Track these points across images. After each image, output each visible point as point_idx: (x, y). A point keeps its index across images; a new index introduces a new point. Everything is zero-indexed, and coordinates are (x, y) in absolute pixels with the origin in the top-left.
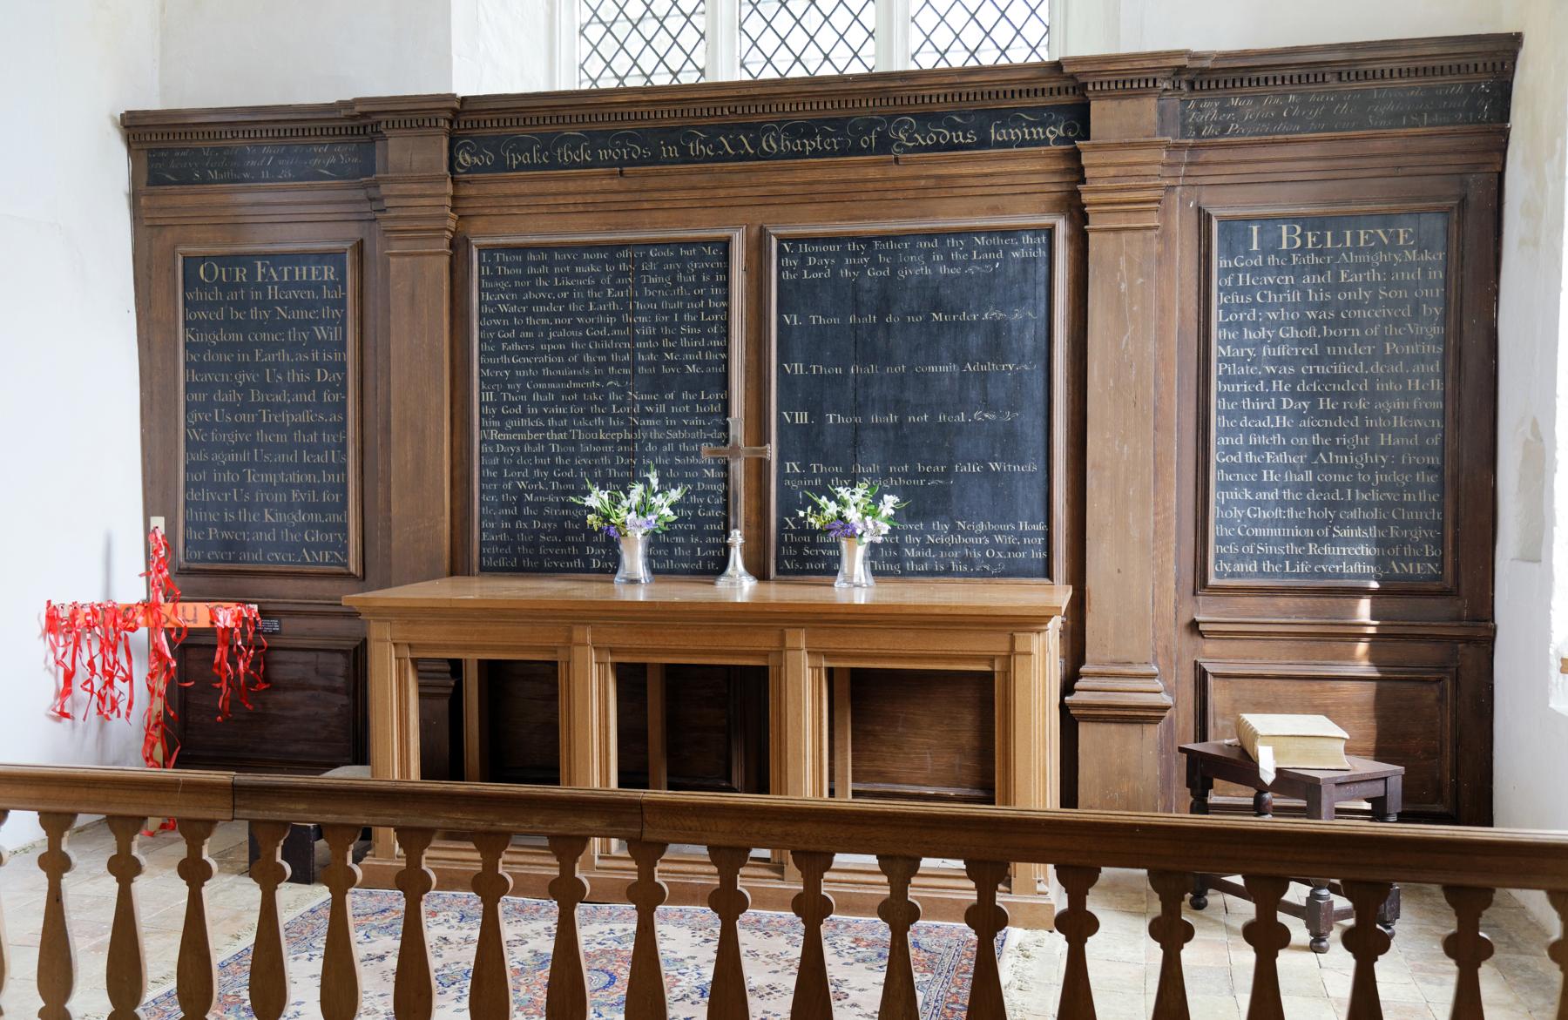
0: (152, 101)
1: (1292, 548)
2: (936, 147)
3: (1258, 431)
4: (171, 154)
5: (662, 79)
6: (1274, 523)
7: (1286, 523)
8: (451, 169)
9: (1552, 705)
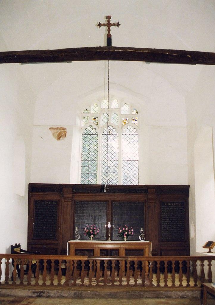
0: (190, 186)
1: (170, 237)
2: (131, 193)
3: (166, 224)
4: (33, 188)
5: (114, 184)
6: (168, 234)
7: (169, 234)
8: (72, 192)
9: (197, 251)
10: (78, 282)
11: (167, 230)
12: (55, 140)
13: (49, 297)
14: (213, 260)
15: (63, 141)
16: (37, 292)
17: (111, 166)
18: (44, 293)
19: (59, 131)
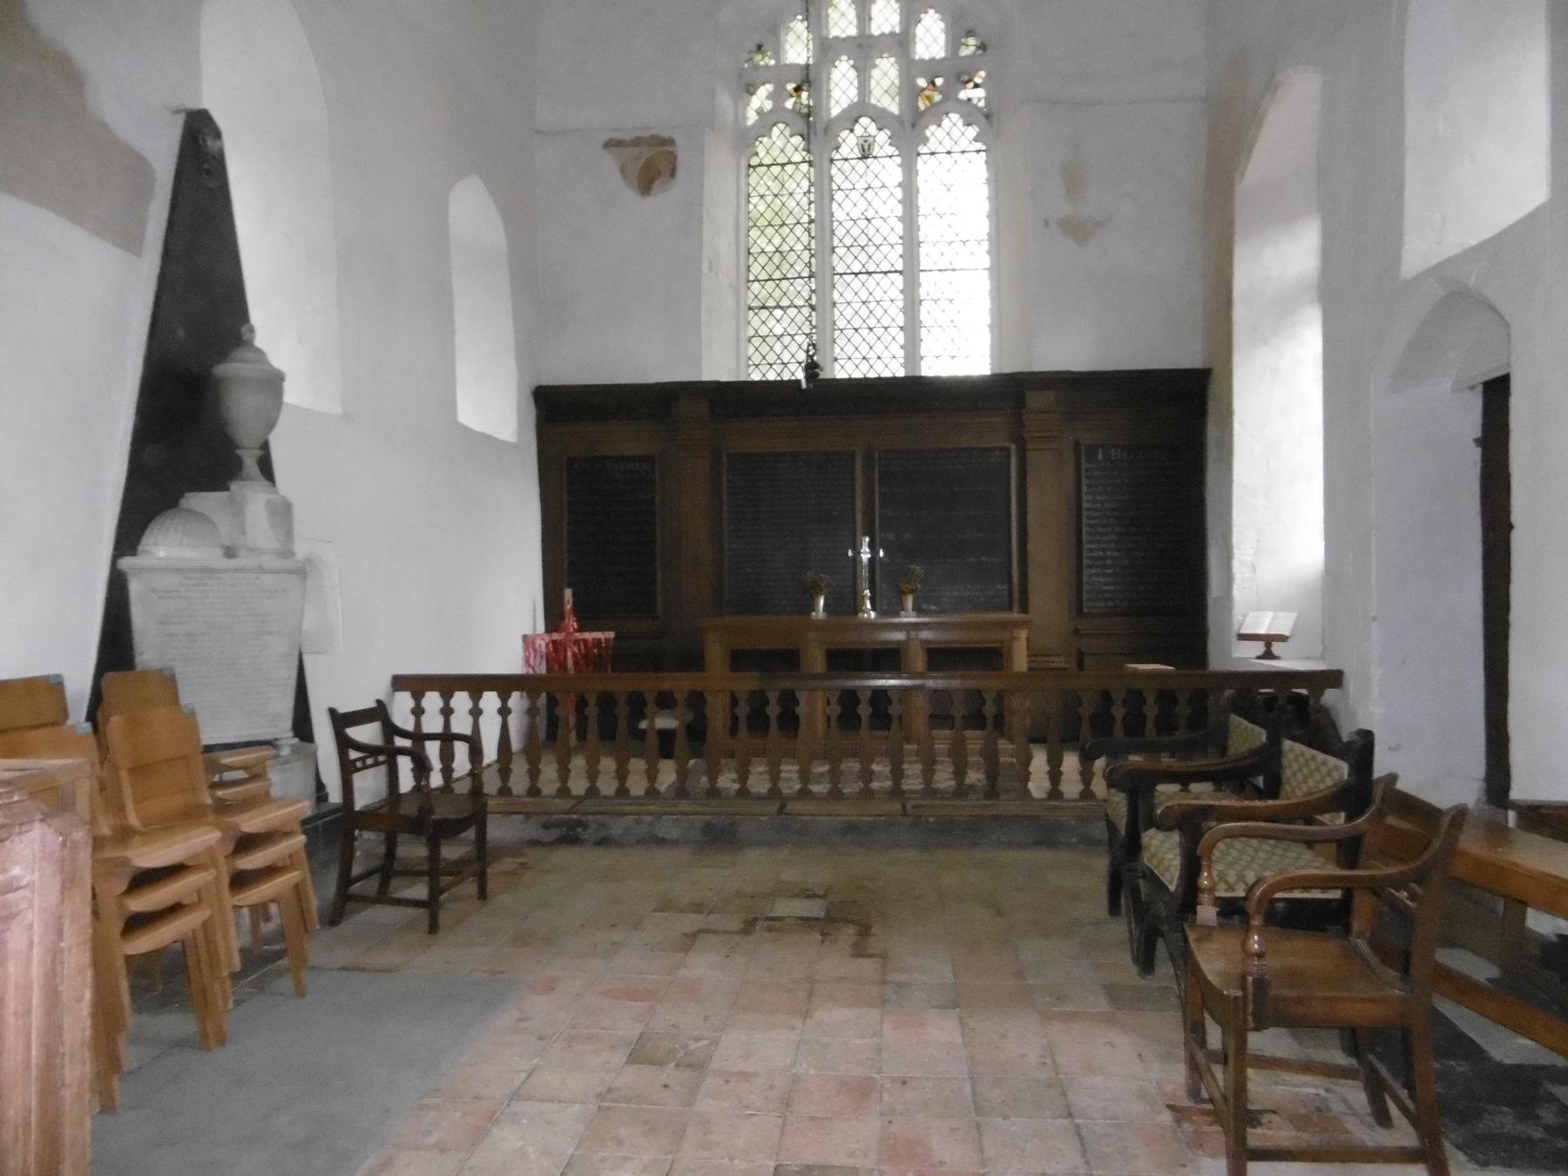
10: (727, 781)
11: (1105, 567)
12: (630, 195)
13: (604, 842)
14: (491, 690)
15: (664, 201)
16: (558, 825)
17: (886, 298)
18: (585, 826)
19: (647, 153)
